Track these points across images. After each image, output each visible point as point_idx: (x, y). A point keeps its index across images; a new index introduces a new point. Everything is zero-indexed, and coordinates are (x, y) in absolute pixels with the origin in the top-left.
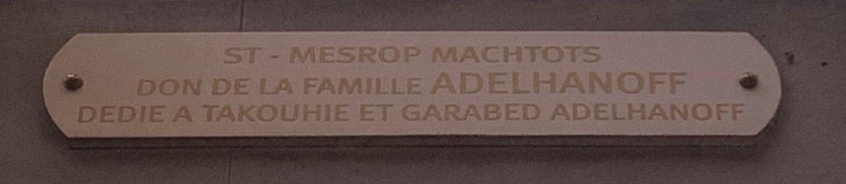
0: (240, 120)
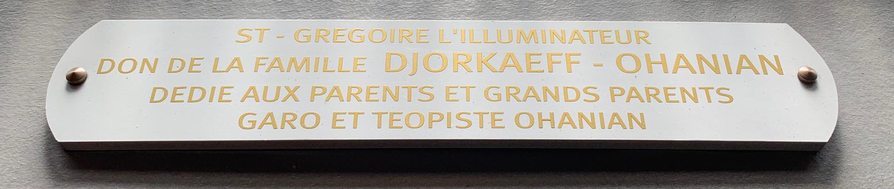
0: (282, 128)
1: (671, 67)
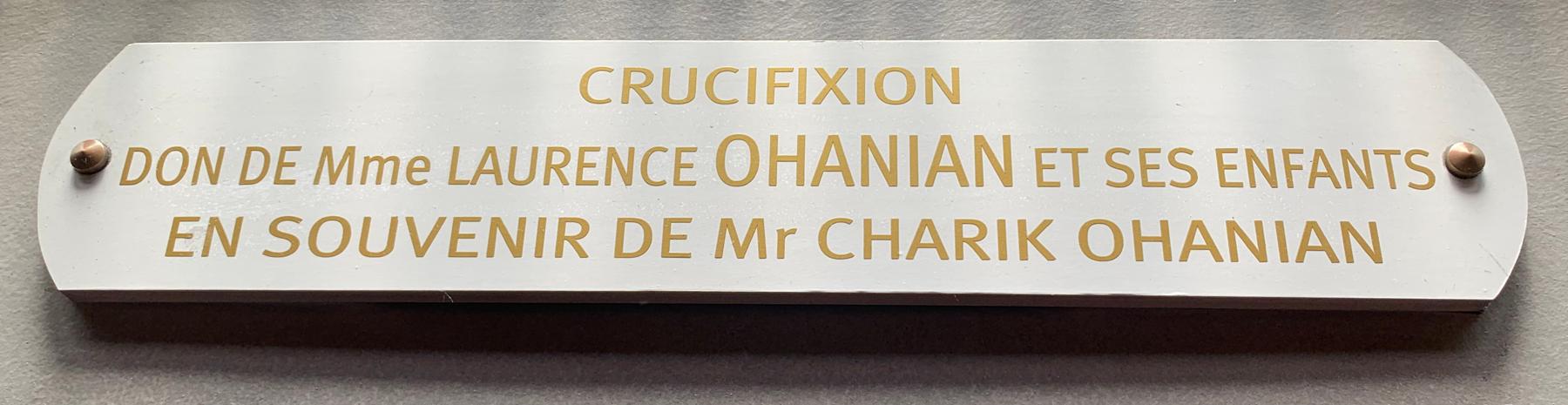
1: (1177, 250)
